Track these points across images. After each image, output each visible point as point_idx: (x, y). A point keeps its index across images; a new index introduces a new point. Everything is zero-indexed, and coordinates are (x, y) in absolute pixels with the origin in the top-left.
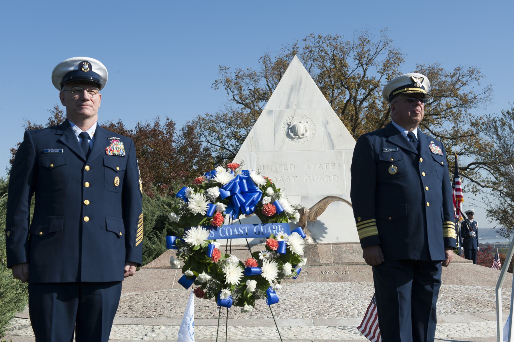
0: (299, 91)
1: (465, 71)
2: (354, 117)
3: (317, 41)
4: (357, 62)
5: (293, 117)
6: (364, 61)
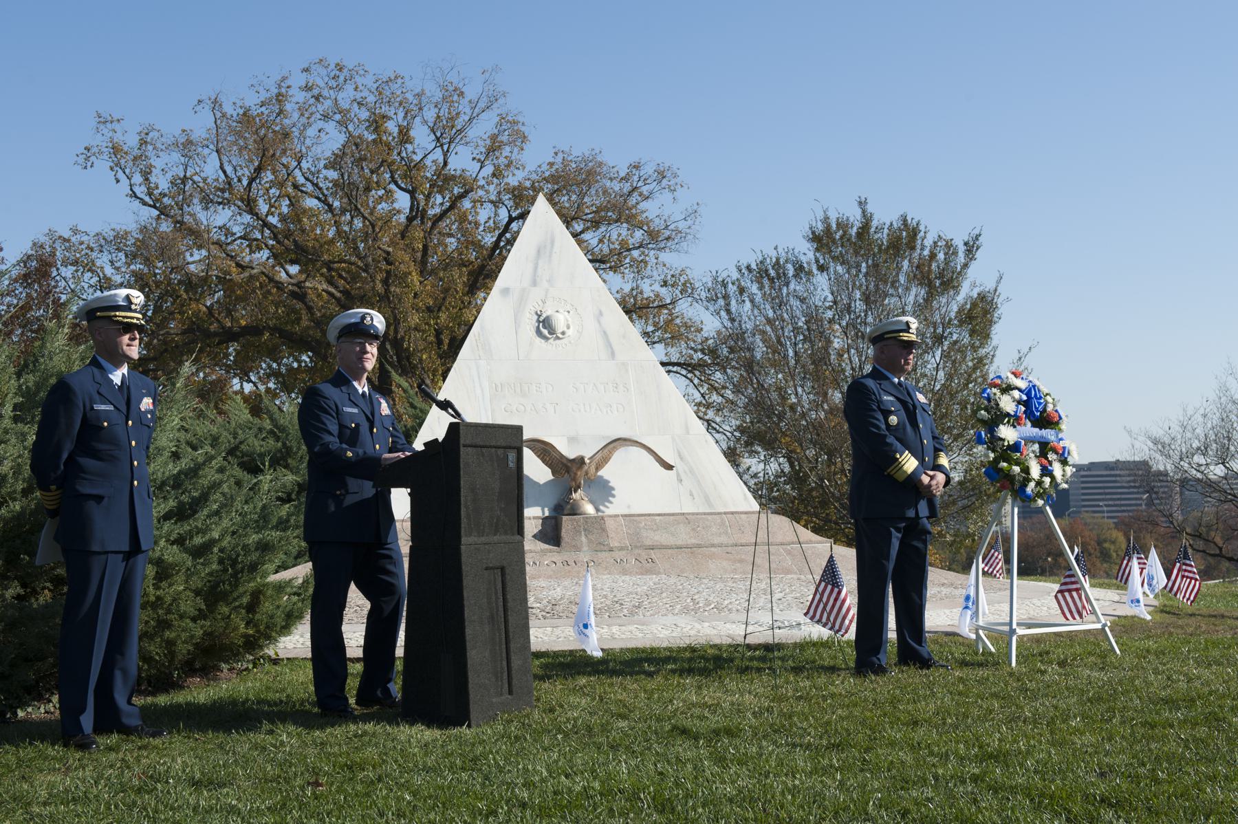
1: (648, 170)
3: (332, 75)
5: (544, 302)
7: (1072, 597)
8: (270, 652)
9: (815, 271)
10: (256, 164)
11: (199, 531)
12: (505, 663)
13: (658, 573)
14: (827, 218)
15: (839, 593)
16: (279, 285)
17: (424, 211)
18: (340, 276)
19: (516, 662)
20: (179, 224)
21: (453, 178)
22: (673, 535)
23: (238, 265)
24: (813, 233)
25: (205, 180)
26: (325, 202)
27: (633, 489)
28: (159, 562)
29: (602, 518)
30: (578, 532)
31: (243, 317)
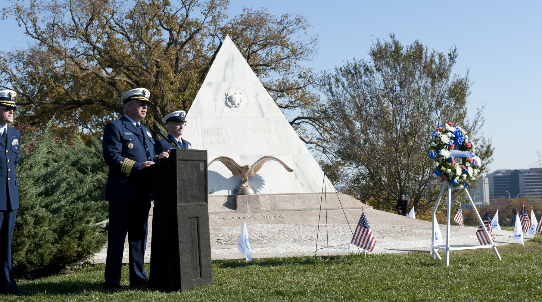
1: (292, 18)
5: (229, 89)
7: (481, 234)
8: (90, 260)
9: (375, 71)
10: (90, 16)
11: (56, 201)
12: (198, 262)
13: (285, 223)
14: (379, 43)
15: (368, 231)
16: (102, 79)
17: (176, 40)
18: (134, 74)
19: (204, 262)
20: (51, 48)
21: (191, 23)
22: (293, 204)
23: (81, 68)
24: (373, 51)
25: (64, 25)
26: (126, 35)
27: (274, 182)
28: (36, 216)
29: (257, 196)
30: (245, 203)
31: (84, 95)
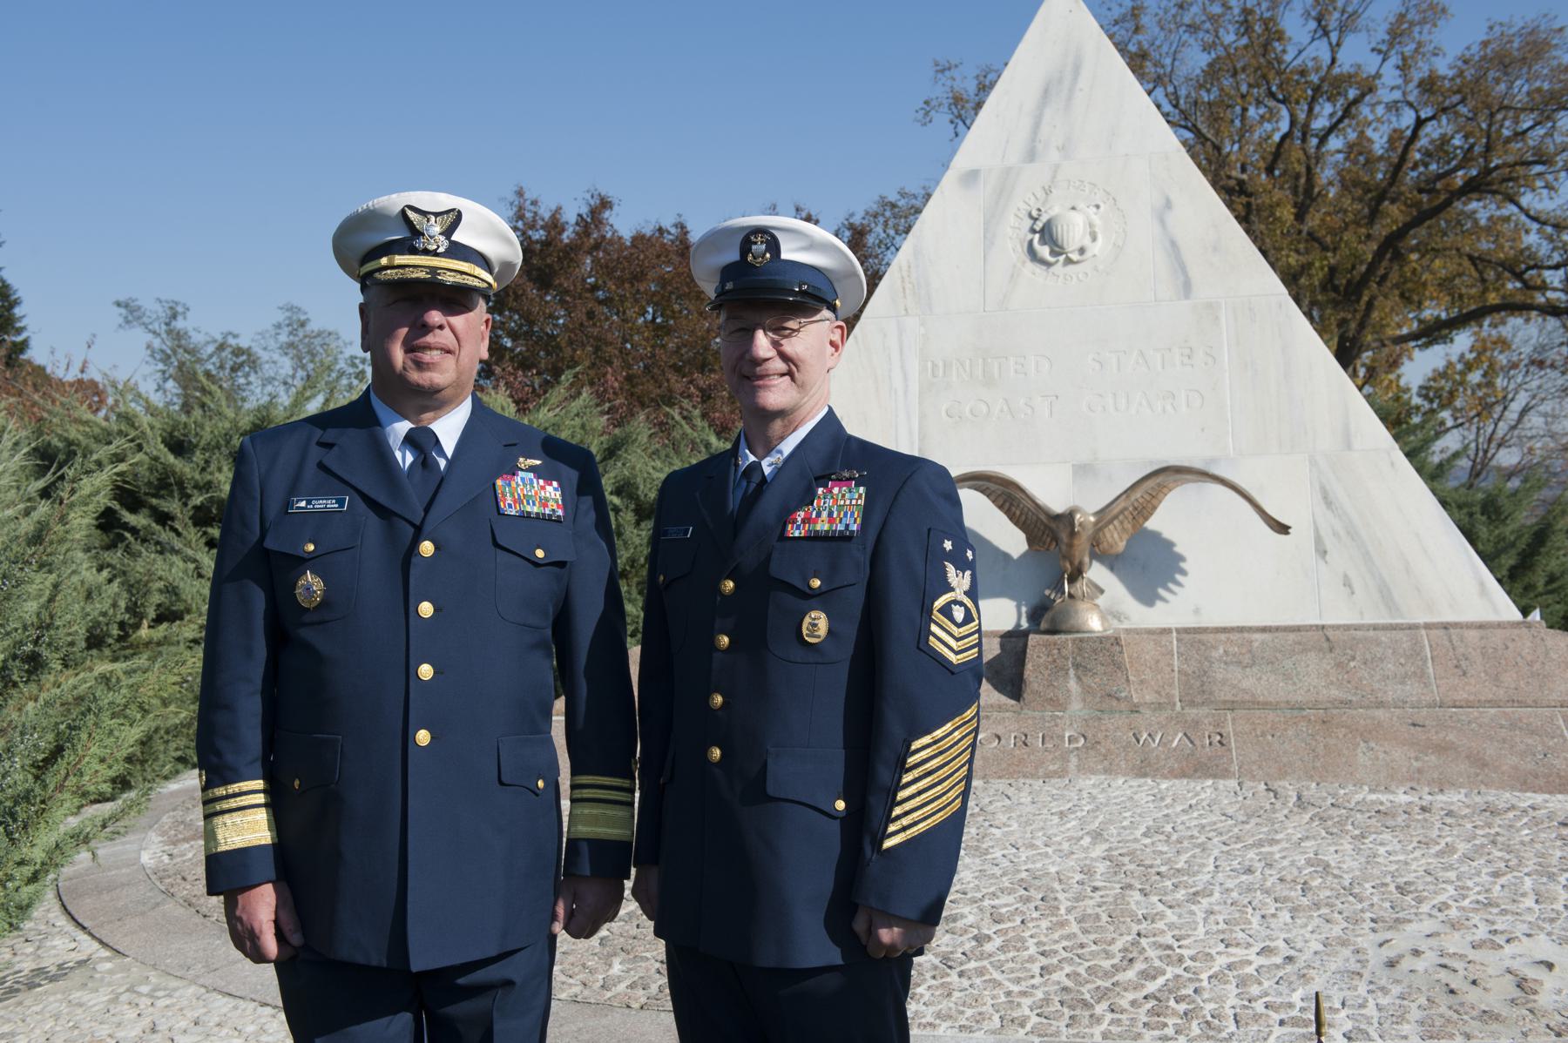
0: (1070, 98)
2: (1303, 180)
4: (1313, 25)
5: (1048, 192)
6: (1333, 20)
